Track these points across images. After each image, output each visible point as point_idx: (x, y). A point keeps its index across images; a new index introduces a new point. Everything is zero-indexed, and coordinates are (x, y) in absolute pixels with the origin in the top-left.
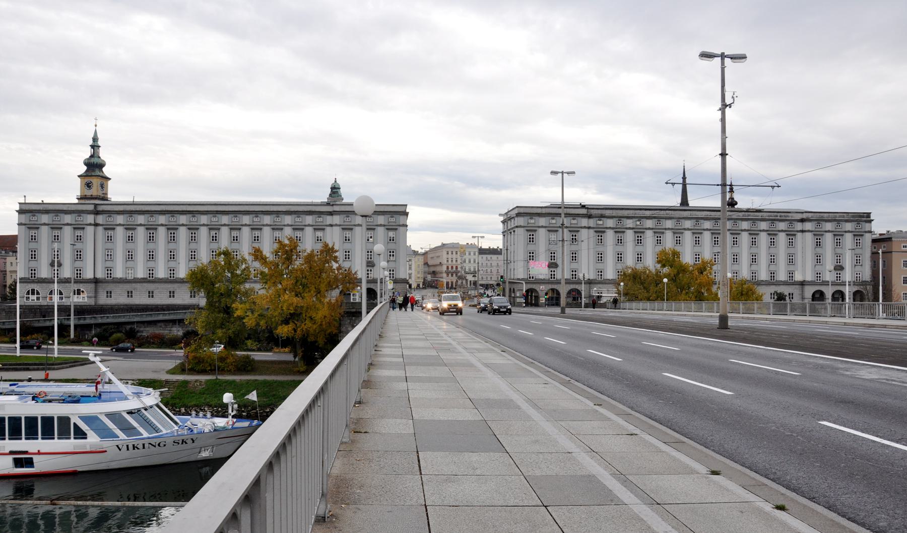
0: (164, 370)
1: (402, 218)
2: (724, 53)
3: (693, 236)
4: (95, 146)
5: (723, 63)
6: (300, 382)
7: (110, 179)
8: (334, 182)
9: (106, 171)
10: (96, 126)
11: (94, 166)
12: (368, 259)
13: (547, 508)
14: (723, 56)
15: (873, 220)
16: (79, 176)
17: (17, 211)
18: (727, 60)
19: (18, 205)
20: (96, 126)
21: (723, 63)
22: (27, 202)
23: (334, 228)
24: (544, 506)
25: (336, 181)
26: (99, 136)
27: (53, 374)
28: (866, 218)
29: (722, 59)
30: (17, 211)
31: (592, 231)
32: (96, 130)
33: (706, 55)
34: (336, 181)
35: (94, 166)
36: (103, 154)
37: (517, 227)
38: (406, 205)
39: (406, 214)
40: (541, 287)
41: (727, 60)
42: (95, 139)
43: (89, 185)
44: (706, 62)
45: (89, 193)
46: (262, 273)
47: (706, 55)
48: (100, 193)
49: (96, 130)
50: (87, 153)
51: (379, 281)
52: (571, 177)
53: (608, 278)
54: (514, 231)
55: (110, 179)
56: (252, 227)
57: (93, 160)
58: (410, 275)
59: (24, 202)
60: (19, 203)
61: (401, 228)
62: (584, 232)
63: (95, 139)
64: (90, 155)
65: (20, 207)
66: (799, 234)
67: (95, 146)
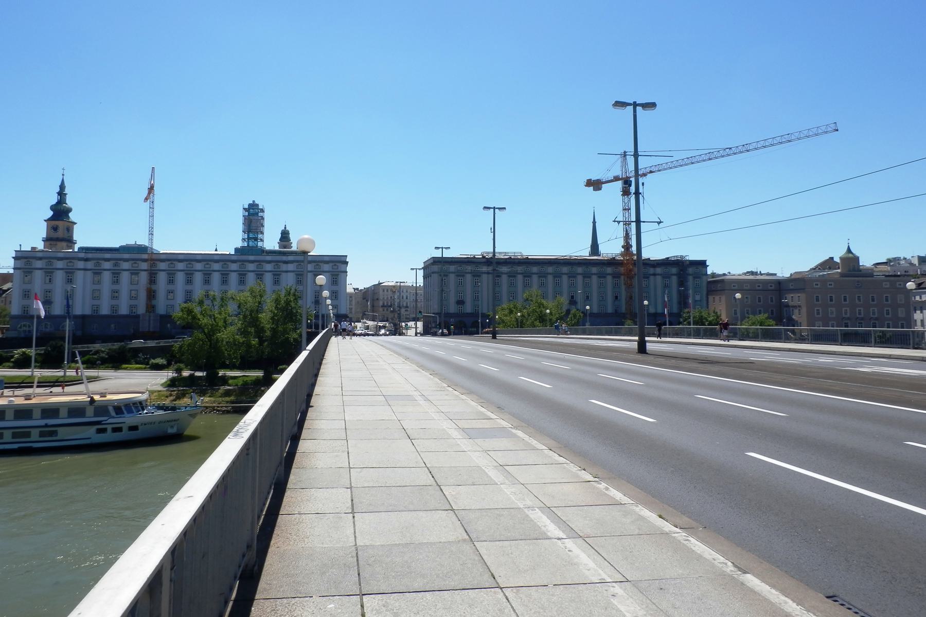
0: (159, 384)
1: (344, 266)
2: (636, 102)
3: (569, 280)
4: (62, 193)
5: (635, 111)
6: (251, 407)
7: (76, 223)
8: (283, 228)
9: (72, 216)
10: (63, 175)
11: (60, 212)
12: (316, 298)
13: (502, 591)
14: (635, 105)
15: (708, 266)
16: (45, 220)
17: (13, 258)
18: (639, 109)
19: (14, 252)
20: (63, 175)
21: (635, 111)
22: (22, 250)
23: (289, 274)
24: (501, 588)
25: (285, 228)
26: (66, 184)
27: (67, 389)
28: (703, 264)
29: (634, 107)
30: (13, 258)
31: (89, 273)
32: (63, 180)
33: (619, 104)
34: (285, 228)
35: (60, 212)
36: (70, 202)
37: (433, 273)
38: (346, 256)
39: (347, 263)
40: (451, 320)
41: (639, 109)
42: (62, 187)
43: (55, 229)
44: (619, 111)
45: (55, 235)
46: (259, 308)
47: (619, 104)
48: (66, 236)
49: (63, 180)
50: (54, 200)
51: (325, 316)
52: (649, 113)
53: (467, 312)
54: (431, 276)
55: (76, 223)
56: (256, 273)
57: (59, 207)
58: (351, 309)
59: (19, 250)
60: (16, 251)
61: (343, 274)
62: (485, 277)
63: (62, 187)
64: (57, 201)
65: (16, 254)
66: (652, 278)
67: (62, 193)
